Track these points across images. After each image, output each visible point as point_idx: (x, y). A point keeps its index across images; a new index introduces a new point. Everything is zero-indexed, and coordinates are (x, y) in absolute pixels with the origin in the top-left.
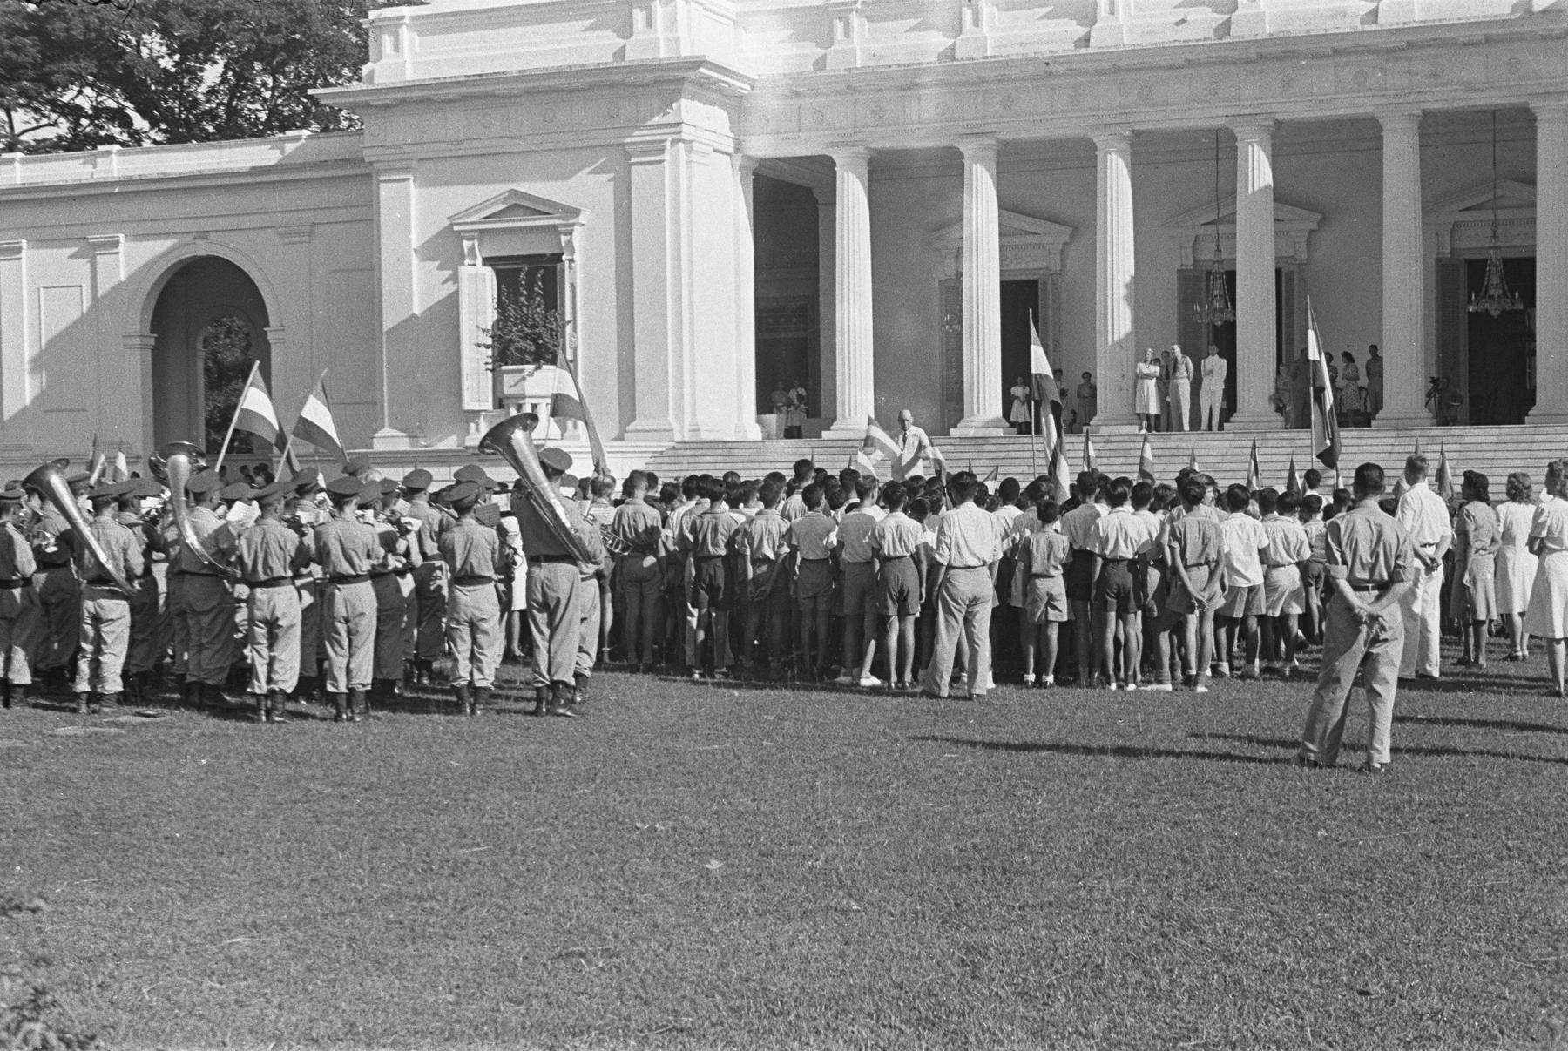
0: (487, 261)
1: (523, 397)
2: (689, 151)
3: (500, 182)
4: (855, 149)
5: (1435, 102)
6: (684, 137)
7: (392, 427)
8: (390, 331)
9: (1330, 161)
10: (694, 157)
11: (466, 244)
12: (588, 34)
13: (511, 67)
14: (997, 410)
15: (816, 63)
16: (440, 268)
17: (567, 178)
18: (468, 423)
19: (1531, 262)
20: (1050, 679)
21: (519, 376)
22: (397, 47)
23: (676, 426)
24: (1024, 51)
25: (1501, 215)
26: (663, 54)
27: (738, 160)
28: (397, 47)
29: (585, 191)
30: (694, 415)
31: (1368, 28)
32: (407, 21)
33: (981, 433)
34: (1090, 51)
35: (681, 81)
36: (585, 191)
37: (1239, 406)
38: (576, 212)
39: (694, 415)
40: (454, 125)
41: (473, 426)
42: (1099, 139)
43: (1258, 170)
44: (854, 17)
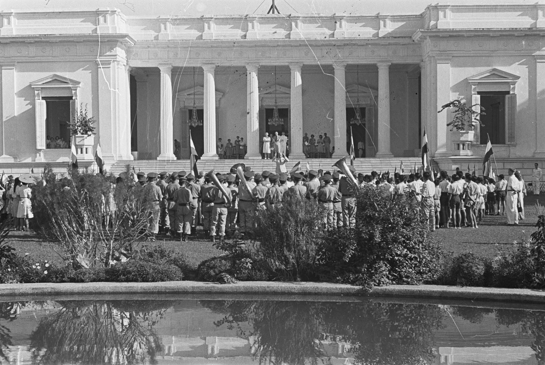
0: (43, 98)
1: (83, 145)
2: (118, 64)
3: (47, 71)
4: (168, 66)
5: (396, 61)
6: (117, 60)
7: (6, 154)
8: (5, 122)
9: (318, 77)
10: (119, 66)
11: (36, 92)
12: (82, 23)
13: (57, 33)
14: (215, 152)
15: (155, 37)
16: (25, 100)
17: (74, 71)
18: (36, 154)
19: (203, 110)
20: (438, 226)
21: (81, 139)
22: (9, 23)
23: (115, 156)
24: (232, 38)
25: (277, 96)
26: (111, 32)
27: (128, 68)
28: (9, 23)
29: (82, 76)
30: (119, 152)
31: (331, 39)
32: (13, 14)
33: (211, 158)
34: (246, 40)
35: (118, 41)
36: (82, 76)
37: (379, 149)
38: (79, 83)
39: (119, 152)
40: (33, 51)
41: (38, 155)
42: (248, 68)
43: (297, 80)
44: (168, 24)
